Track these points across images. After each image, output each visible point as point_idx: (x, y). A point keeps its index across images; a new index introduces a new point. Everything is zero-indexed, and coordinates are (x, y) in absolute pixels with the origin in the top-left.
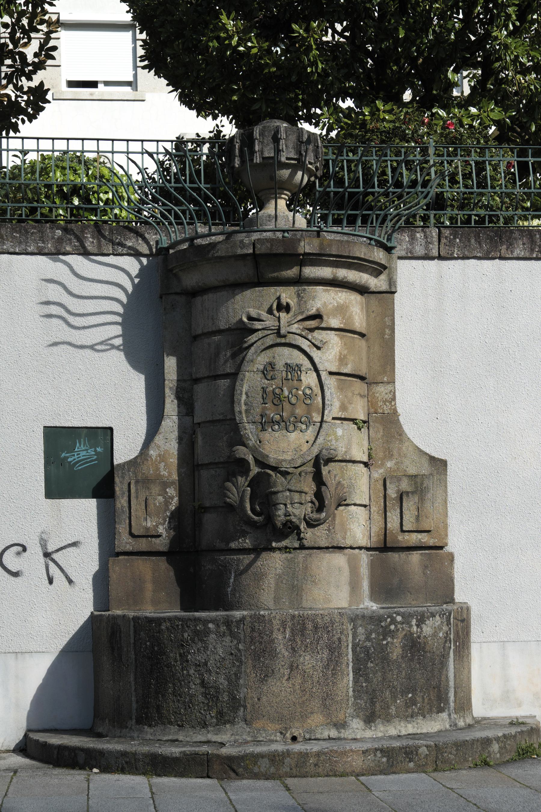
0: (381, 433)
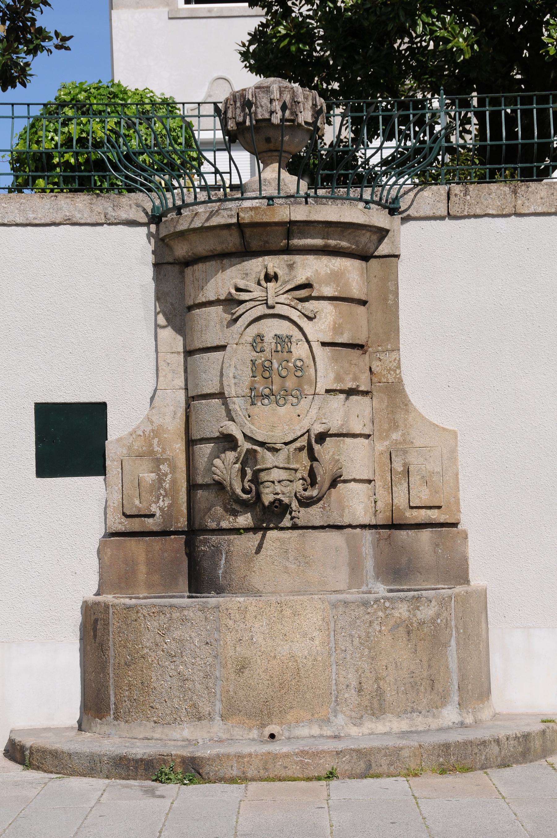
0: (386, 404)
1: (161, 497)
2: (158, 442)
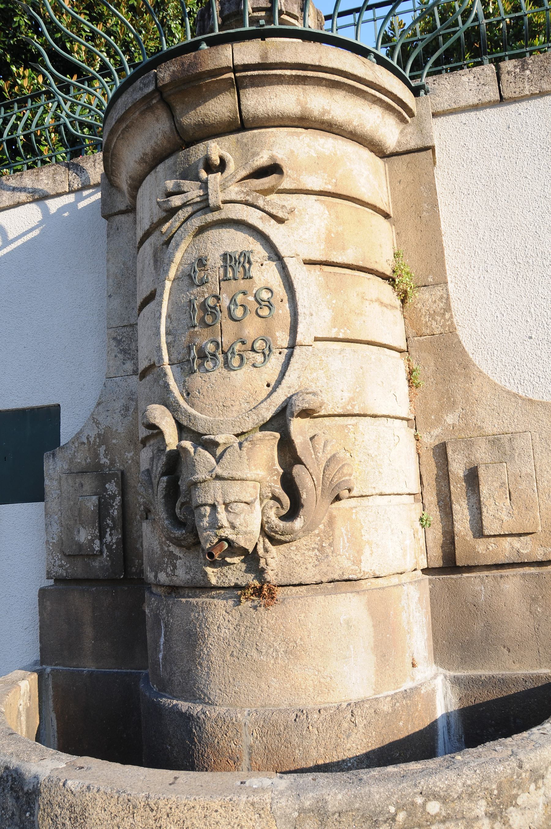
1: (108, 530)
2: (105, 451)
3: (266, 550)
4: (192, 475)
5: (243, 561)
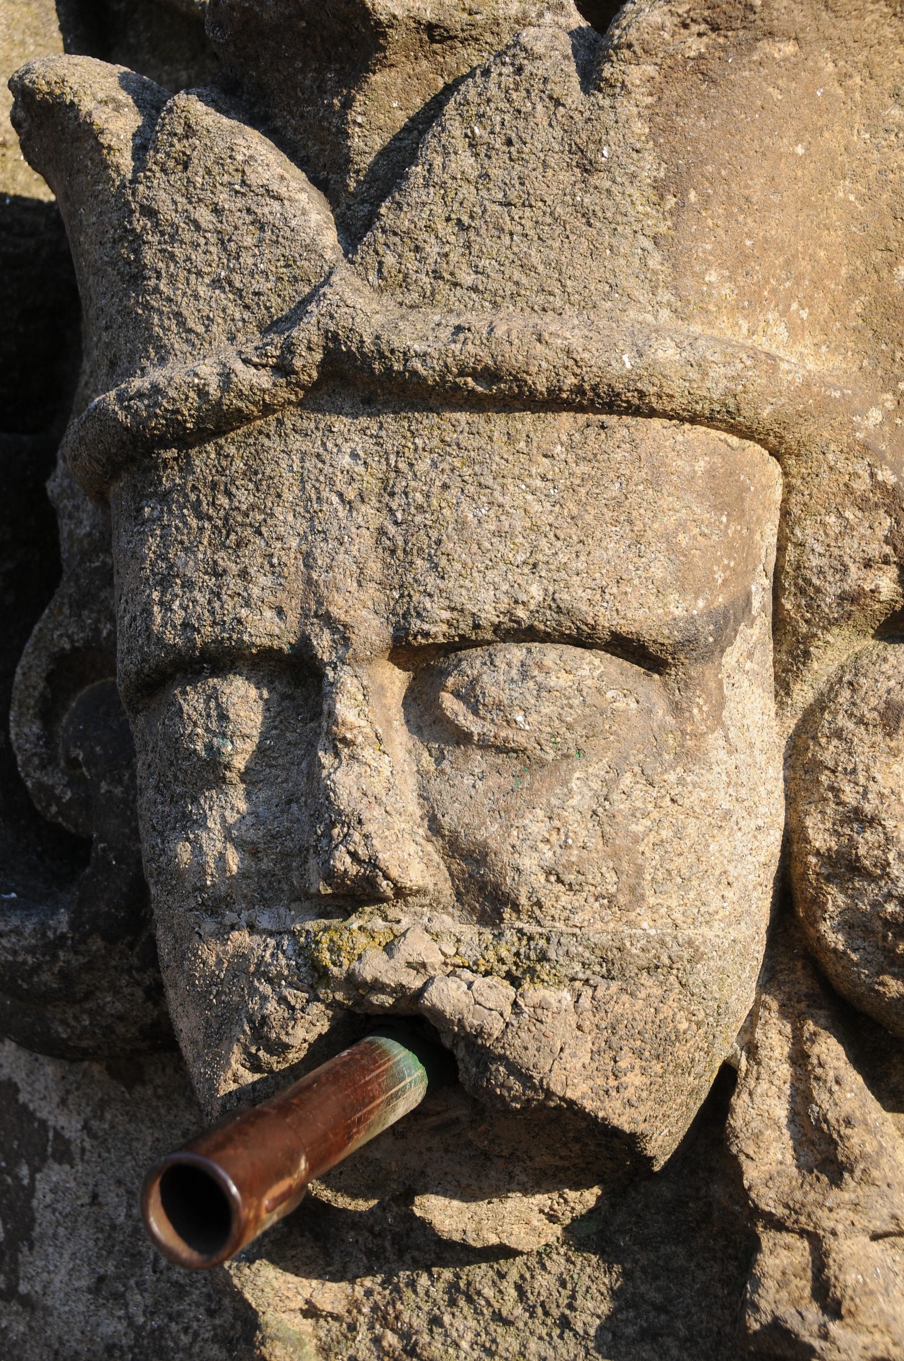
3: (822, 1153)
4: (120, 366)
5: (583, 1235)
